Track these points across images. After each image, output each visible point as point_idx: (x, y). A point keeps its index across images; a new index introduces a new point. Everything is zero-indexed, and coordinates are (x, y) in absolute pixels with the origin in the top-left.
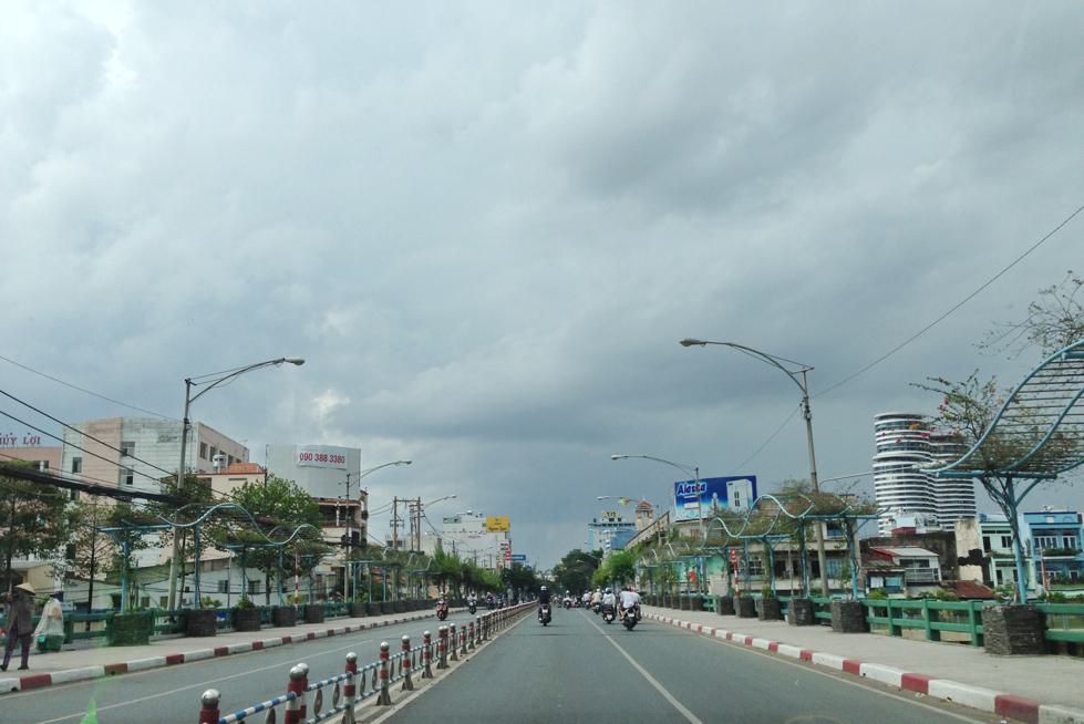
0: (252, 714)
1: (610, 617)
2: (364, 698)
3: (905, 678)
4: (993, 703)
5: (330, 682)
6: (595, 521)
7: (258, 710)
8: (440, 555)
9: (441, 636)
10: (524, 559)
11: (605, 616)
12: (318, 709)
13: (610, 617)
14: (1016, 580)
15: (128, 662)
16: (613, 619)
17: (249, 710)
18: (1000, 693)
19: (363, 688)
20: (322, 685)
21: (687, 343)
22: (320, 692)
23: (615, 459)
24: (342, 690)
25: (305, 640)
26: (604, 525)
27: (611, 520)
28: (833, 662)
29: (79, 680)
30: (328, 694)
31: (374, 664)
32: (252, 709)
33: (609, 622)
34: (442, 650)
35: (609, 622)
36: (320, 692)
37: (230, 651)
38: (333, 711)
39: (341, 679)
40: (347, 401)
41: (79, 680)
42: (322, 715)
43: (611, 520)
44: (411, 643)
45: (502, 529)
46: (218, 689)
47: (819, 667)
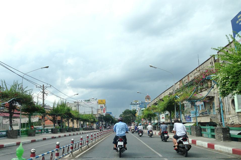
0: (46, 154)
1: (141, 134)
2: (75, 150)
3: (233, 150)
4: (232, 150)
5: (78, 142)
6: (132, 103)
7: (48, 153)
8: (15, 92)
9: (72, 143)
10: (111, 114)
11: (139, 134)
12: (75, 147)
13: (141, 134)
14: (222, 122)
15: (4, 144)
16: (142, 135)
17: (65, 146)
18: (234, 148)
19: (75, 147)
20: (64, 147)
21: (151, 66)
22: (76, 145)
23: (138, 92)
24: (70, 148)
25: (30, 143)
28: (220, 148)
29: (12, 146)
30: (66, 149)
31: (78, 142)
32: (46, 153)
33: (140, 136)
34: (238, 60)
35: (140, 136)
36: (76, 145)
37: (46, 139)
38: (78, 148)
39: (79, 142)
40: (73, 80)
41: (12, 146)
42: (76, 149)
44: (60, 145)
45: (103, 103)
46: (35, 149)
47: (198, 146)
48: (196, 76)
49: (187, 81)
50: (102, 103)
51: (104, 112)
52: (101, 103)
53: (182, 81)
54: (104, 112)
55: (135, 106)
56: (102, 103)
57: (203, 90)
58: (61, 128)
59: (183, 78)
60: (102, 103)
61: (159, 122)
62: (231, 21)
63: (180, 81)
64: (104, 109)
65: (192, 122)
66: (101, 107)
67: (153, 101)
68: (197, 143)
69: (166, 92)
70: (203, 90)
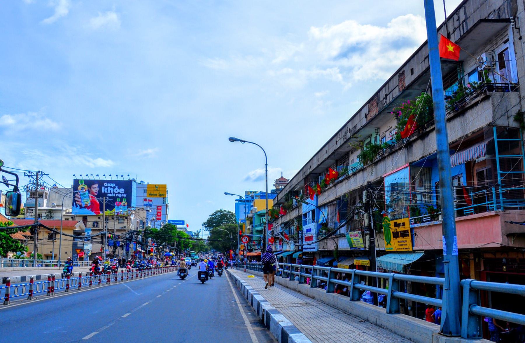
45: (160, 195)
50: (157, 193)
51: (160, 218)
52: (155, 193)
54: (160, 218)
56: (156, 195)
60: (157, 193)
64: (159, 211)
66: (146, 203)
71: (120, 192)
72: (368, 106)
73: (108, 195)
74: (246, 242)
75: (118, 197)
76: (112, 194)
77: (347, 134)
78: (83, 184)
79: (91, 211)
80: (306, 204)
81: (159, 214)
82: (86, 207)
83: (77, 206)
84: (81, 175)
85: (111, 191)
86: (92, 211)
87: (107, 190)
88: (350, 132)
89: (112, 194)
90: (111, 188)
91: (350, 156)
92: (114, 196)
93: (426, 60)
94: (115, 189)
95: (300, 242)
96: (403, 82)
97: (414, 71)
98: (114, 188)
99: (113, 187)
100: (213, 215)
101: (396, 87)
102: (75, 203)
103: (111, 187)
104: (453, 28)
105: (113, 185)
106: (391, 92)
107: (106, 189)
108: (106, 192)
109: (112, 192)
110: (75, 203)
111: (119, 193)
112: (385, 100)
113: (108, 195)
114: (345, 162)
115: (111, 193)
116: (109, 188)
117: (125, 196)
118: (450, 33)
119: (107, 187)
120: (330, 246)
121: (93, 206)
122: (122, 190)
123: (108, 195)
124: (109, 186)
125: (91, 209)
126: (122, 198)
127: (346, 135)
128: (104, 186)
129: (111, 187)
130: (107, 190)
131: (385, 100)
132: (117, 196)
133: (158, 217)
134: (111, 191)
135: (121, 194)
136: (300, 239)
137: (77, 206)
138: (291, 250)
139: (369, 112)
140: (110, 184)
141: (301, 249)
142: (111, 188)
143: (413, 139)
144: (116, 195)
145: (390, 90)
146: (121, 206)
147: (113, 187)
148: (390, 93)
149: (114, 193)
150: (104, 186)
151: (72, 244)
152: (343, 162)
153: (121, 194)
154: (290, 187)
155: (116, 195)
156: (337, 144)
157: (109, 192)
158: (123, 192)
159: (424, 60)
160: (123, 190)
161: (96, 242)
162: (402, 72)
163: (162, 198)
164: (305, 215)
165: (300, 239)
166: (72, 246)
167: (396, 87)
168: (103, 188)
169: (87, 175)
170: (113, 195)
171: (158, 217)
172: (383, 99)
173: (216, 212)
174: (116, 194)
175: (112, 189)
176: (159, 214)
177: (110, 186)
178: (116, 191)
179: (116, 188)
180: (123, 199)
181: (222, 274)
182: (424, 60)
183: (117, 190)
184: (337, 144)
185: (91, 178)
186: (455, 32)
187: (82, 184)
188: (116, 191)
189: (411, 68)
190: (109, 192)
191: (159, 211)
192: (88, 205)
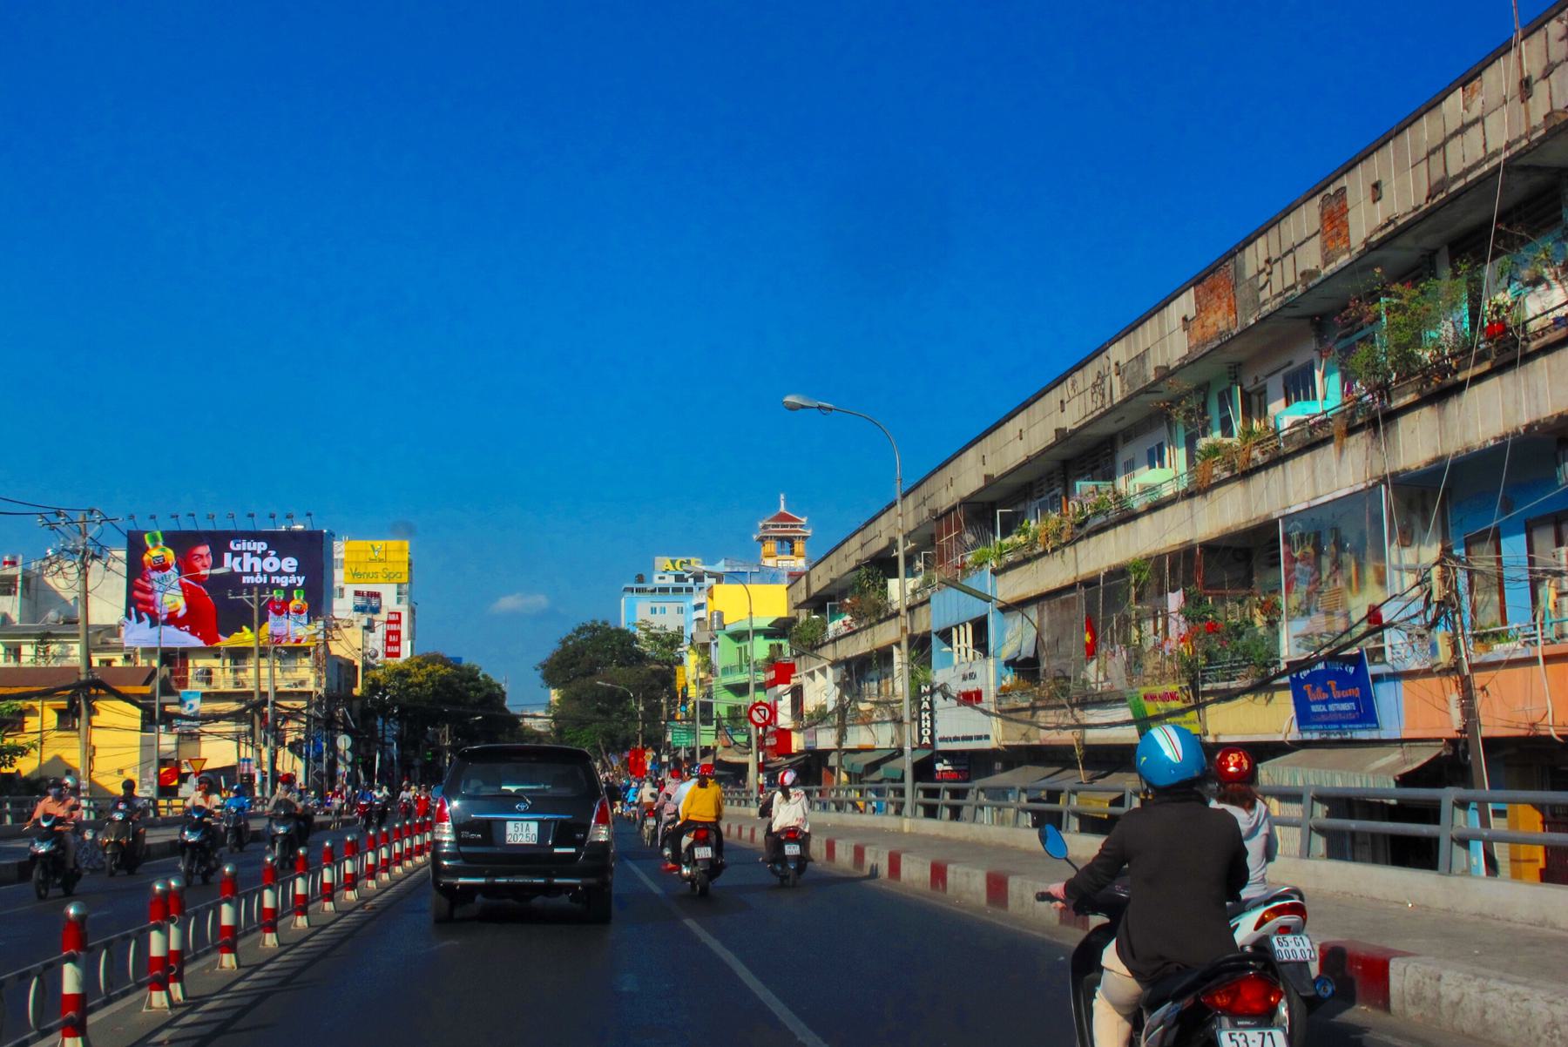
26: (664, 590)
27: (679, 578)
43: (679, 578)
48: (1452, 172)
49: (1310, 257)
50: (379, 567)
51: (396, 649)
52: (372, 568)
53: (1239, 271)
54: (396, 649)
55: (671, 608)
57: (284, 711)
58: (567, 737)
59: (1249, 241)
61: (926, 740)
62: (228, 637)
63: (1197, 281)
64: (393, 627)
65: (1384, 735)
66: (374, 602)
67: (855, 543)
68: (836, 857)
69: (1011, 428)
70: (284, 711)
71: (286, 569)
72: (1196, 293)
73: (244, 578)
74: (763, 721)
75: (277, 586)
76: (259, 576)
77: (1107, 379)
78: (161, 544)
79: (186, 634)
80: (985, 601)
81: (393, 639)
82: (173, 620)
83: (140, 620)
84: (153, 517)
85: (252, 565)
86: (193, 632)
87: (241, 564)
88: (1118, 374)
89: (259, 576)
90: (252, 556)
91: (1119, 449)
92: (265, 582)
93: (1432, 157)
94: (267, 561)
95: (926, 720)
96: (1337, 222)
97: (1385, 190)
98: (264, 555)
99: (259, 552)
100: (570, 638)
101: (1308, 238)
102: (133, 610)
103: (254, 554)
104: (1545, 63)
105: (261, 547)
106: (1290, 251)
107: (237, 560)
108: (237, 569)
109: (257, 569)
110: (133, 610)
111: (280, 573)
112: (1263, 278)
113: (246, 580)
114: (1097, 467)
115: (253, 573)
116: (247, 556)
117: (301, 580)
118: (1530, 77)
119: (239, 554)
120: (1051, 730)
121: (192, 620)
122: (290, 564)
123: (244, 578)
124: (247, 551)
125: (187, 627)
126: (290, 589)
127: (1103, 382)
128: (229, 550)
129: (254, 554)
130: (241, 564)
131: (1263, 278)
132: (273, 582)
133: (390, 649)
134: (252, 565)
135: (289, 575)
136: (926, 710)
137: (140, 620)
138: (877, 747)
139: (1199, 311)
140: (249, 544)
141: (929, 742)
142: (252, 556)
143: (1401, 402)
144: (269, 580)
145: (1286, 247)
146: (288, 613)
147: (259, 552)
148: (1285, 255)
149: (263, 572)
150: (229, 550)
151: (139, 743)
152: (1091, 466)
153: (289, 575)
154: (863, 545)
155: (269, 580)
156: (1063, 411)
157: (247, 569)
158: (294, 570)
159: (1424, 154)
160: (294, 562)
161: (211, 733)
162: (1337, 191)
163: (396, 586)
164: (946, 635)
165: (926, 710)
166: (138, 749)
167: (1308, 238)
168: (227, 556)
169: (189, 515)
170: (259, 579)
171: (390, 649)
172: (1256, 272)
173: (580, 631)
174: (270, 575)
175: (257, 560)
176: (393, 639)
177: (250, 549)
178: (271, 564)
179: (268, 555)
180: (295, 592)
181: (1035, 825)
182: (1428, 157)
183: (273, 563)
184: (1063, 411)
185: (187, 525)
186: (1552, 76)
187: (156, 546)
188: (271, 564)
189: (1373, 182)
190: (247, 569)
191: (393, 627)
192: (181, 613)
